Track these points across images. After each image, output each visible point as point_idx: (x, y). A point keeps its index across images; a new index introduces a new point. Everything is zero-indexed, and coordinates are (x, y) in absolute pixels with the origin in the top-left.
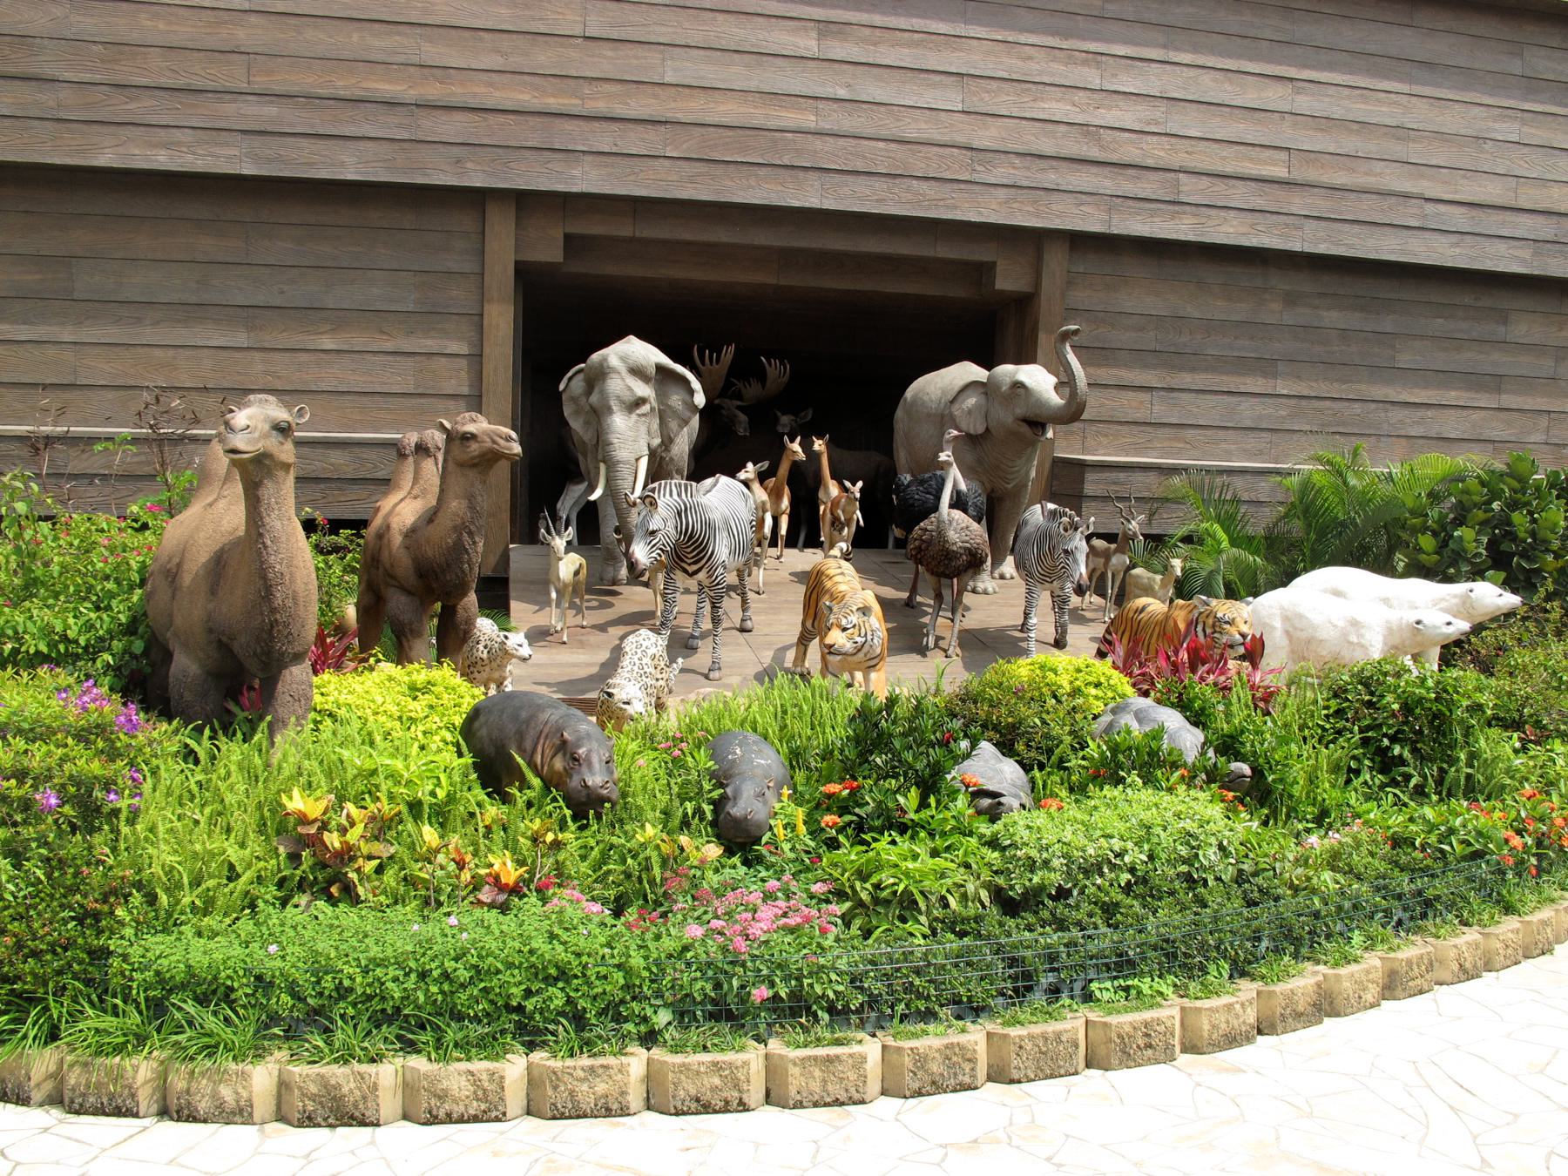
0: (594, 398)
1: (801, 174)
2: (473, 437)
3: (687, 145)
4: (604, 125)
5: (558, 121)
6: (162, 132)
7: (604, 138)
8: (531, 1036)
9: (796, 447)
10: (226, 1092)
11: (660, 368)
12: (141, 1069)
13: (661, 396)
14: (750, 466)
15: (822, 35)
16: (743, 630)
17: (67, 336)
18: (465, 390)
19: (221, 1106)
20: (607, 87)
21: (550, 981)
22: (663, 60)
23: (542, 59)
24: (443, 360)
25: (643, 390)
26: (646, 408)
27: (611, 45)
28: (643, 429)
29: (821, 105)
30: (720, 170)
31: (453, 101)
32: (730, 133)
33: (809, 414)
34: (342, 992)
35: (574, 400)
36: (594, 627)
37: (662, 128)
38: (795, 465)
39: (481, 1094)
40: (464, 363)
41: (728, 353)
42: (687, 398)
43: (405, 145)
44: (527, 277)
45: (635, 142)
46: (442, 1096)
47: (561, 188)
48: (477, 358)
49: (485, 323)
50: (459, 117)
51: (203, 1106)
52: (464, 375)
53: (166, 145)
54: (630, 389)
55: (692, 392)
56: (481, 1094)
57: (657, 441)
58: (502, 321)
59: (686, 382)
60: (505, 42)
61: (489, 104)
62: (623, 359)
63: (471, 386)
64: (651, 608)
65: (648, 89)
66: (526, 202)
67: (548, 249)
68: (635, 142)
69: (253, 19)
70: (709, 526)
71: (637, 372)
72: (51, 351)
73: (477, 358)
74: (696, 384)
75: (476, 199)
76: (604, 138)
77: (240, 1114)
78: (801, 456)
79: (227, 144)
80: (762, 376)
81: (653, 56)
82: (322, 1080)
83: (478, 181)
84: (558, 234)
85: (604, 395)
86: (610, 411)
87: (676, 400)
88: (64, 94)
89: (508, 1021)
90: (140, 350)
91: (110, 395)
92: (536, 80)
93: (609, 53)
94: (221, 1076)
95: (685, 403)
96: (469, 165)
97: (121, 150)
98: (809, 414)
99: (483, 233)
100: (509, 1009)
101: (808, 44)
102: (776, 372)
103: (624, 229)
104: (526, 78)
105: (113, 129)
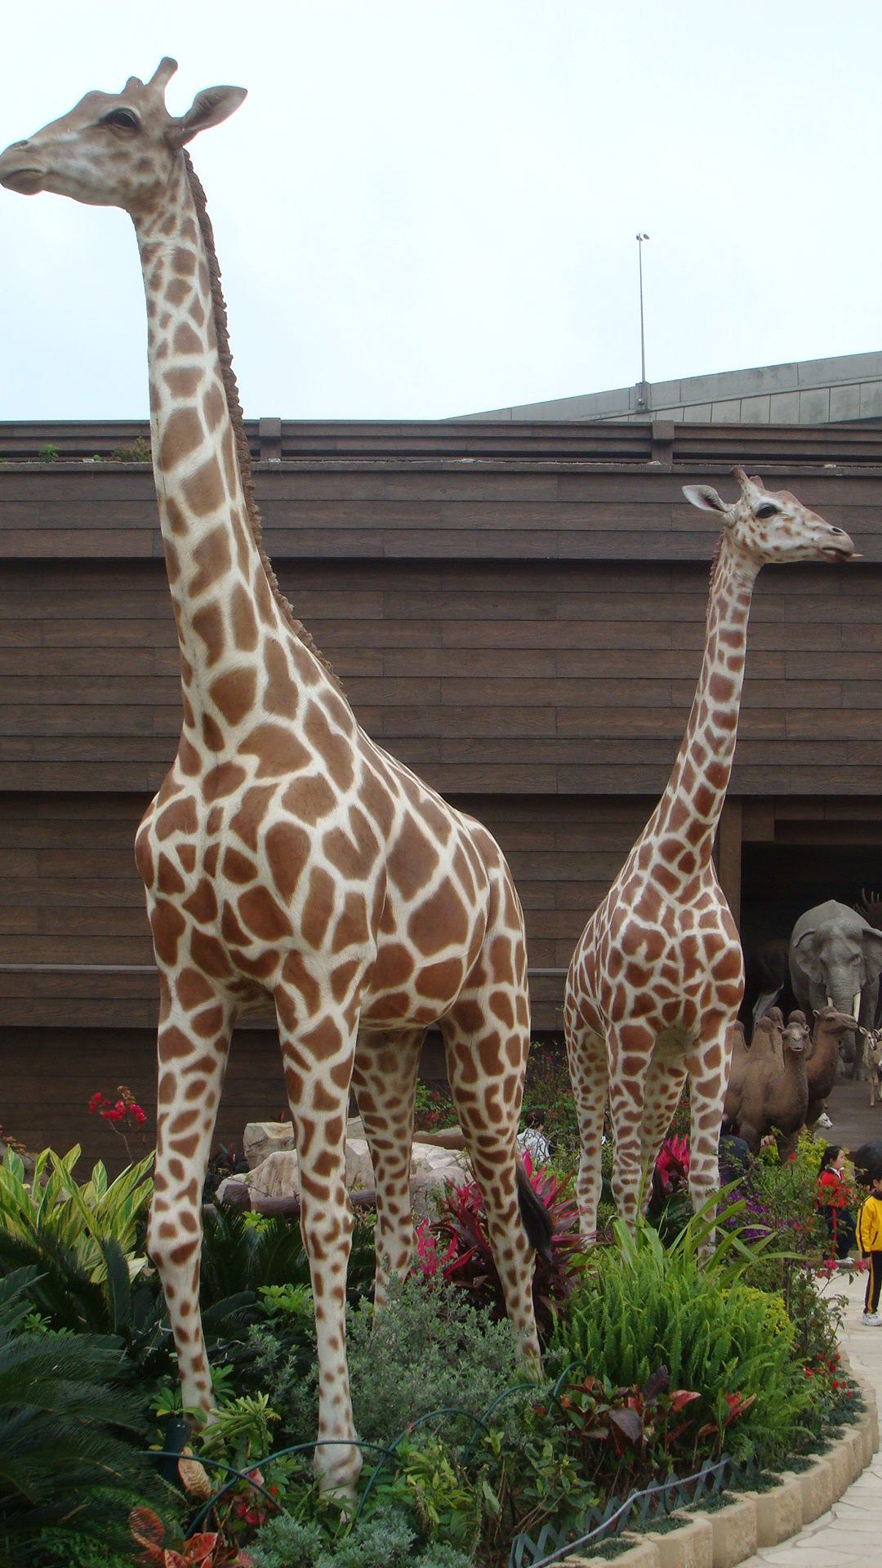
0: (823, 955)
11: (865, 932)
13: (865, 950)
25: (856, 949)
28: (857, 974)
57: (864, 982)
71: (852, 937)
103: (818, 815)
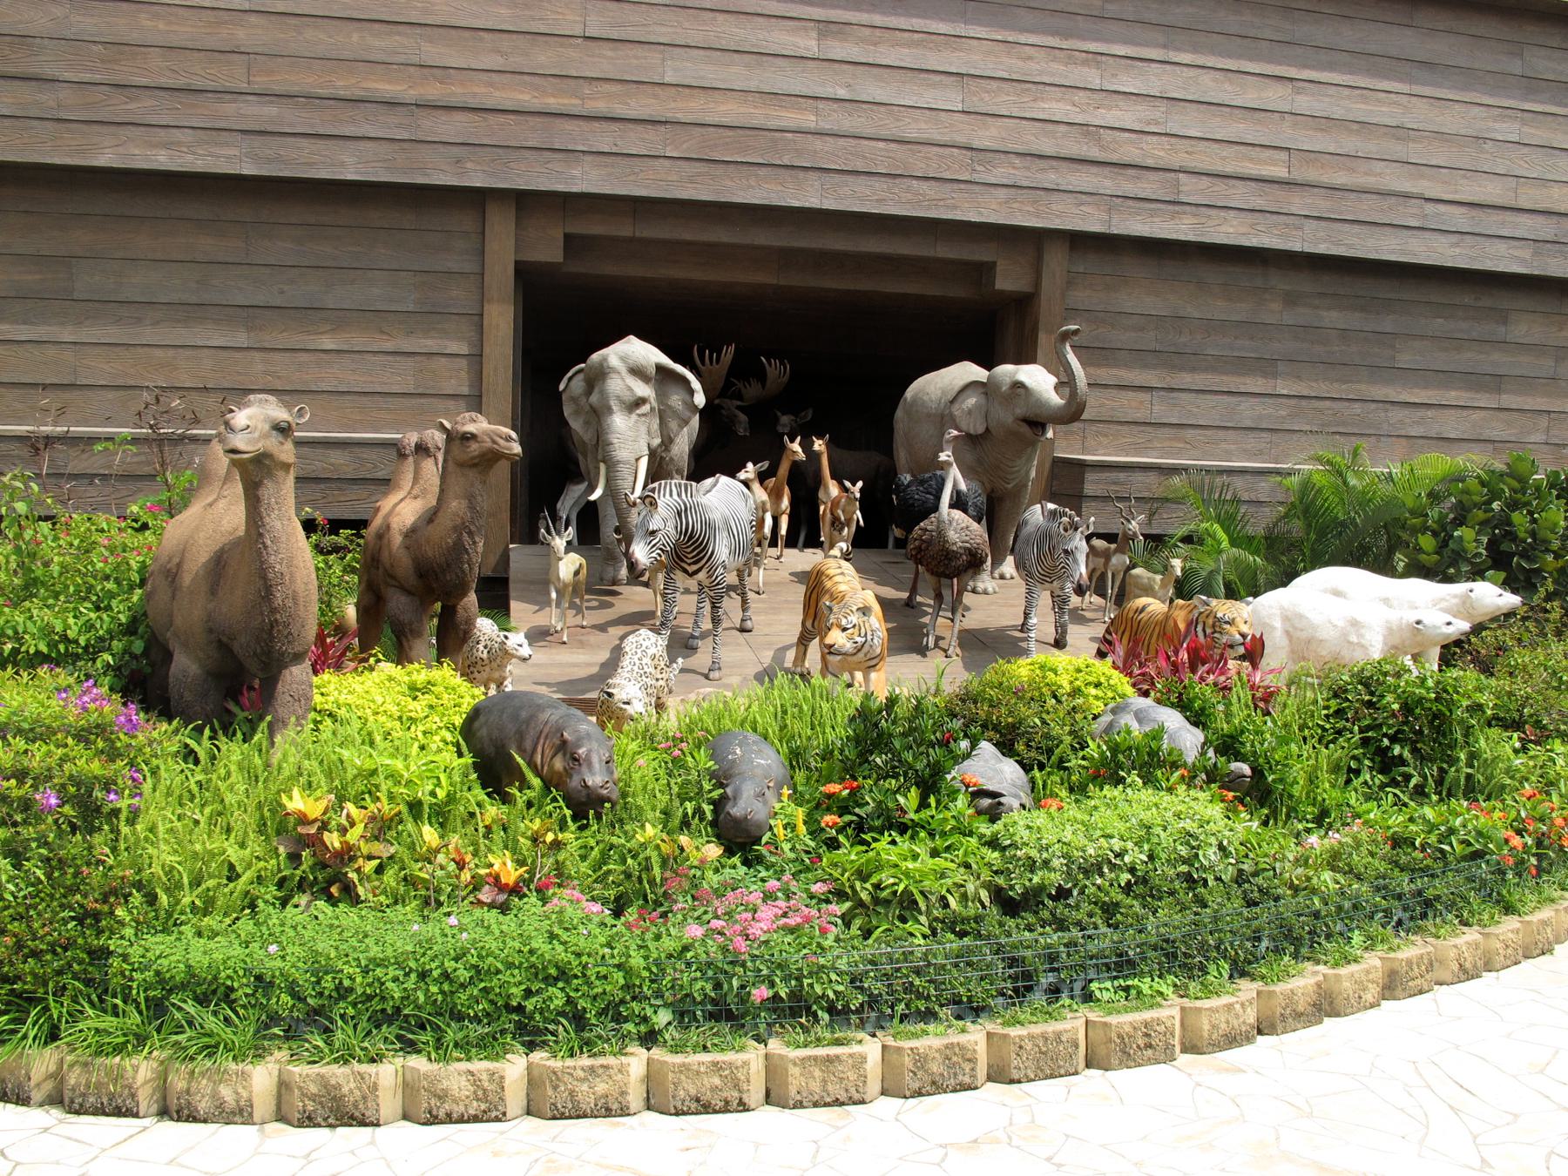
0: (594, 398)
1: (801, 174)
2: (473, 437)
3: (687, 145)
4: (604, 125)
5: (558, 121)
6: (162, 132)
7: (604, 138)
8: (531, 1036)
9: (796, 447)
10: (226, 1092)
11: (660, 368)
12: (141, 1069)
13: (661, 396)
14: (750, 466)
15: (822, 35)
16: (743, 630)
17: (67, 336)
18: (465, 390)
19: (221, 1106)
20: (607, 87)
21: (550, 981)
22: (663, 60)
23: (542, 59)
24: (443, 360)
25: (643, 390)
26: (646, 408)
27: (611, 45)
28: (643, 429)
29: (821, 105)
30: (720, 170)
31: (453, 101)
32: (730, 133)
33: (809, 414)
34: (342, 992)
35: (574, 400)
36: (594, 627)
37: (662, 128)
38: (795, 465)
39: (481, 1094)
40: (464, 363)
41: (728, 353)
42: (687, 398)
43: (405, 145)
44: (527, 277)
45: (635, 142)
46: (442, 1096)
47: (561, 188)
48: (477, 358)
49: (485, 323)
50: (459, 117)
51: (203, 1106)
52: (464, 375)
53: (166, 145)
54: (630, 389)
55: (692, 392)
56: (481, 1094)
57: (657, 441)
58: (502, 321)
59: (686, 382)
60: (505, 42)
61: (489, 104)
62: (623, 359)
63: (471, 386)
64: (651, 608)
65: (648, 89)
66: (526, 202)
67: (548, 249)
68: (635, 142)
69: (253, 19)
70: (709, 526)
71: (637, 372)
72: (51, 351)
73: (477, 358)
74: (696, 384)
75: (476, 199)
76: (604, 138)
77: (240, 1114)
78: (801, 456)
79: (227, 144)
80: (762, 376)
81: (653, 56)
82: (322, 1080)
83: (478, 181)
84: (558, 234)
85: (604, 395)
86: (610, 411)
87: (676, 400)
88: (64, 94)
89: (508, 1021)
90: (140, 350)
91: (110, 395)
92: (536, 80)
93: (609, 53)
94: (221, 1076)
95: (685, 403)
96: (469, 165)
97: (121, 150)
98: (809, 414)
99: (483, 233)
100: (509, 1009)
101: (808, 44)
102: (776, 372)
103: (624, 229)
104: (526, 78)
105: (113, 129)
